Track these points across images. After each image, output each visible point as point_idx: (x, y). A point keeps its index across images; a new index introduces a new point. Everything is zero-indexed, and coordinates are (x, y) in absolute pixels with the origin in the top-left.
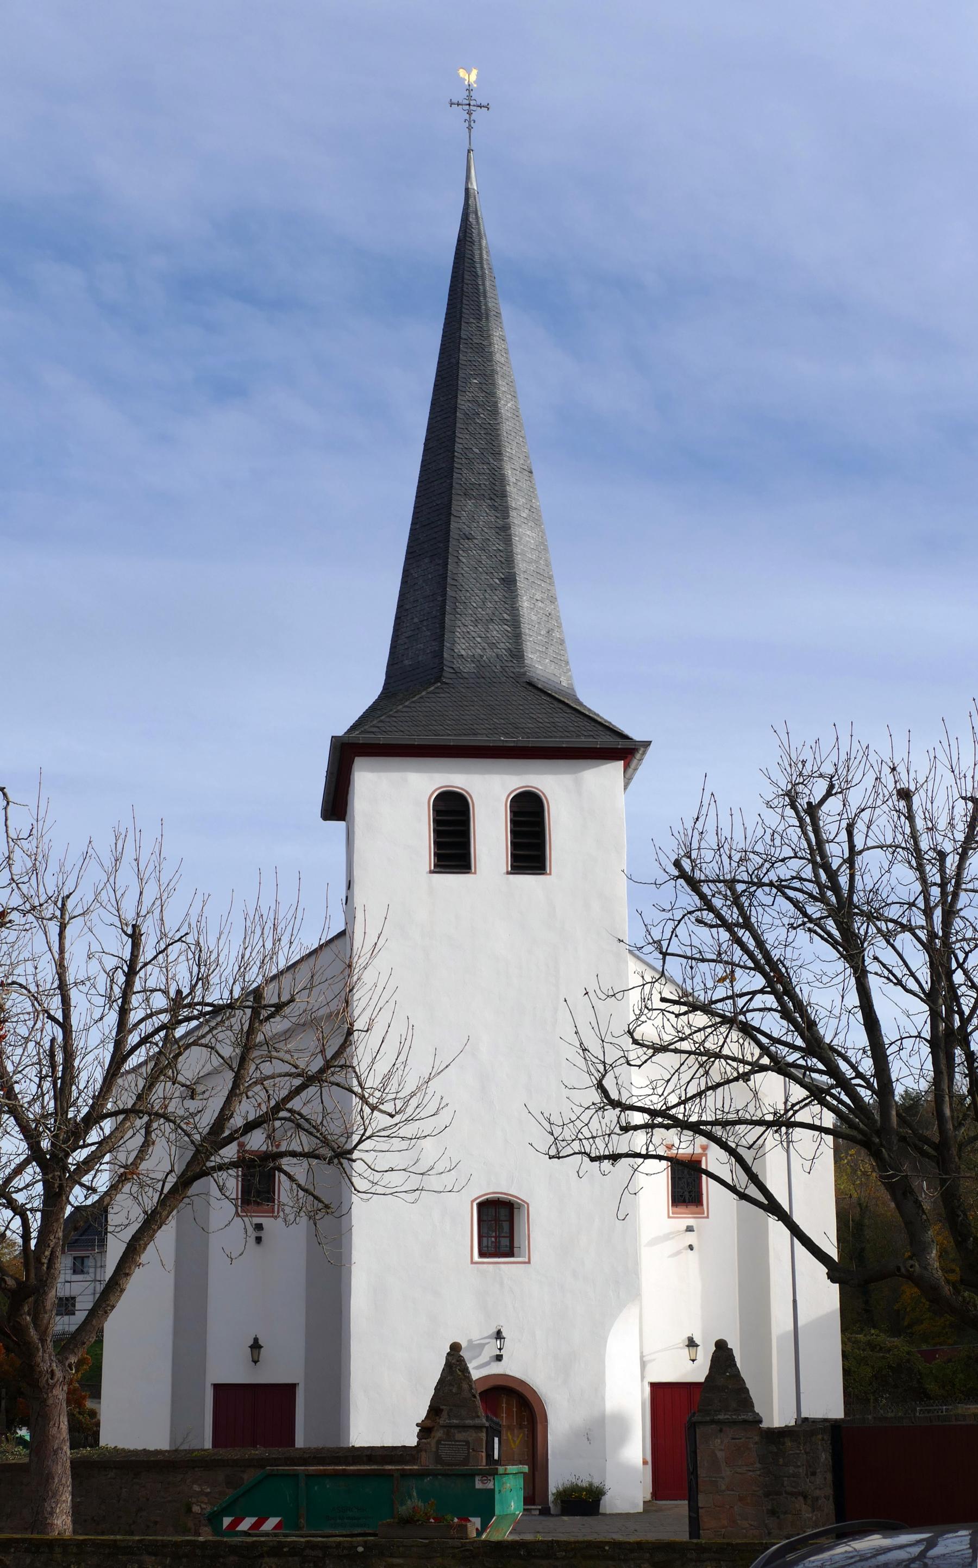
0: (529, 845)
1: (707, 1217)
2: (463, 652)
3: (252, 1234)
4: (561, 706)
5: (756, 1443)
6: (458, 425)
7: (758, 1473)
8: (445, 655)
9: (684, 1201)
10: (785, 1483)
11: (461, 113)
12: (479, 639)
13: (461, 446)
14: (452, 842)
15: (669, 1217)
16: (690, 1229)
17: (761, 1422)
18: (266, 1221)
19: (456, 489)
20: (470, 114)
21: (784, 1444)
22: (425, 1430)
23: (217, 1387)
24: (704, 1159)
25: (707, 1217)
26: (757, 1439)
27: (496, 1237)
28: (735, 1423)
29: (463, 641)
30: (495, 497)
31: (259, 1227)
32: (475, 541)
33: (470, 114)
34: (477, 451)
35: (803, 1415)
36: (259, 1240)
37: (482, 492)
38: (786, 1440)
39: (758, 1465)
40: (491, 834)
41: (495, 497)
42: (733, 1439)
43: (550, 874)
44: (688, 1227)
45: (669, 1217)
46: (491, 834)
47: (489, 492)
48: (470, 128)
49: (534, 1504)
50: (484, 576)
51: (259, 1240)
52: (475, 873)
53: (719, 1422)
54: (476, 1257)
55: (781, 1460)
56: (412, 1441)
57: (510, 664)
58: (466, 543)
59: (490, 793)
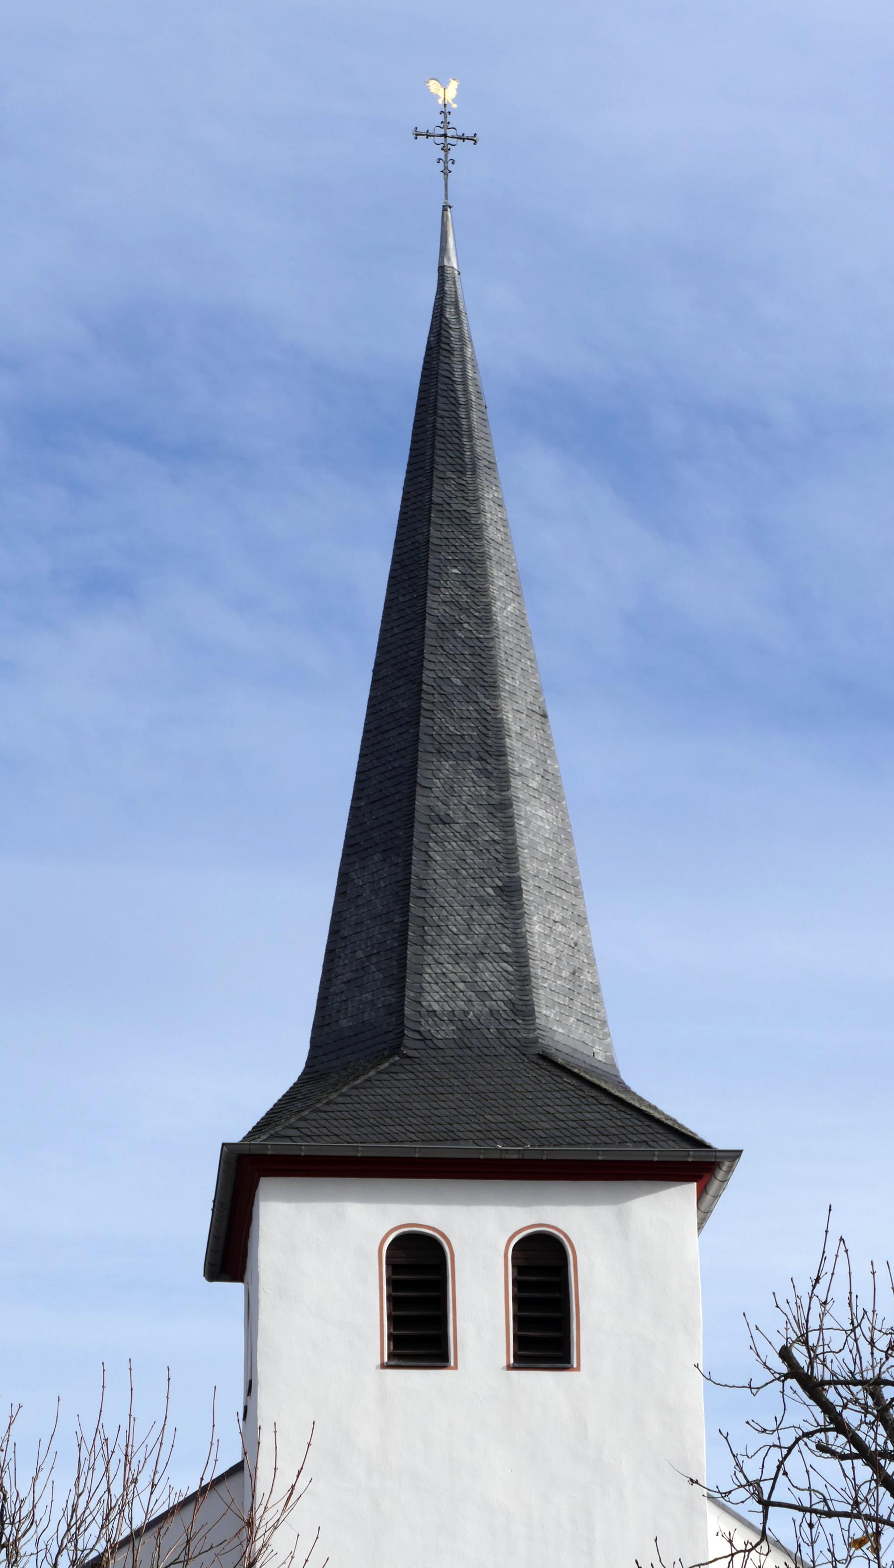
0: (544, 1331)
2: (436, 1007)
4: (594, 1093)
6: (428, 641)
8: (407, 1011)
12: (461, 986)
13: (432, 675)
14: (418, 1326)
30: (487, 757)
32: (456, 827)
40: (481, 1303)
41: (487, 757)
46: (481, 1303)
47: (478, 748)
58: (441, 831)
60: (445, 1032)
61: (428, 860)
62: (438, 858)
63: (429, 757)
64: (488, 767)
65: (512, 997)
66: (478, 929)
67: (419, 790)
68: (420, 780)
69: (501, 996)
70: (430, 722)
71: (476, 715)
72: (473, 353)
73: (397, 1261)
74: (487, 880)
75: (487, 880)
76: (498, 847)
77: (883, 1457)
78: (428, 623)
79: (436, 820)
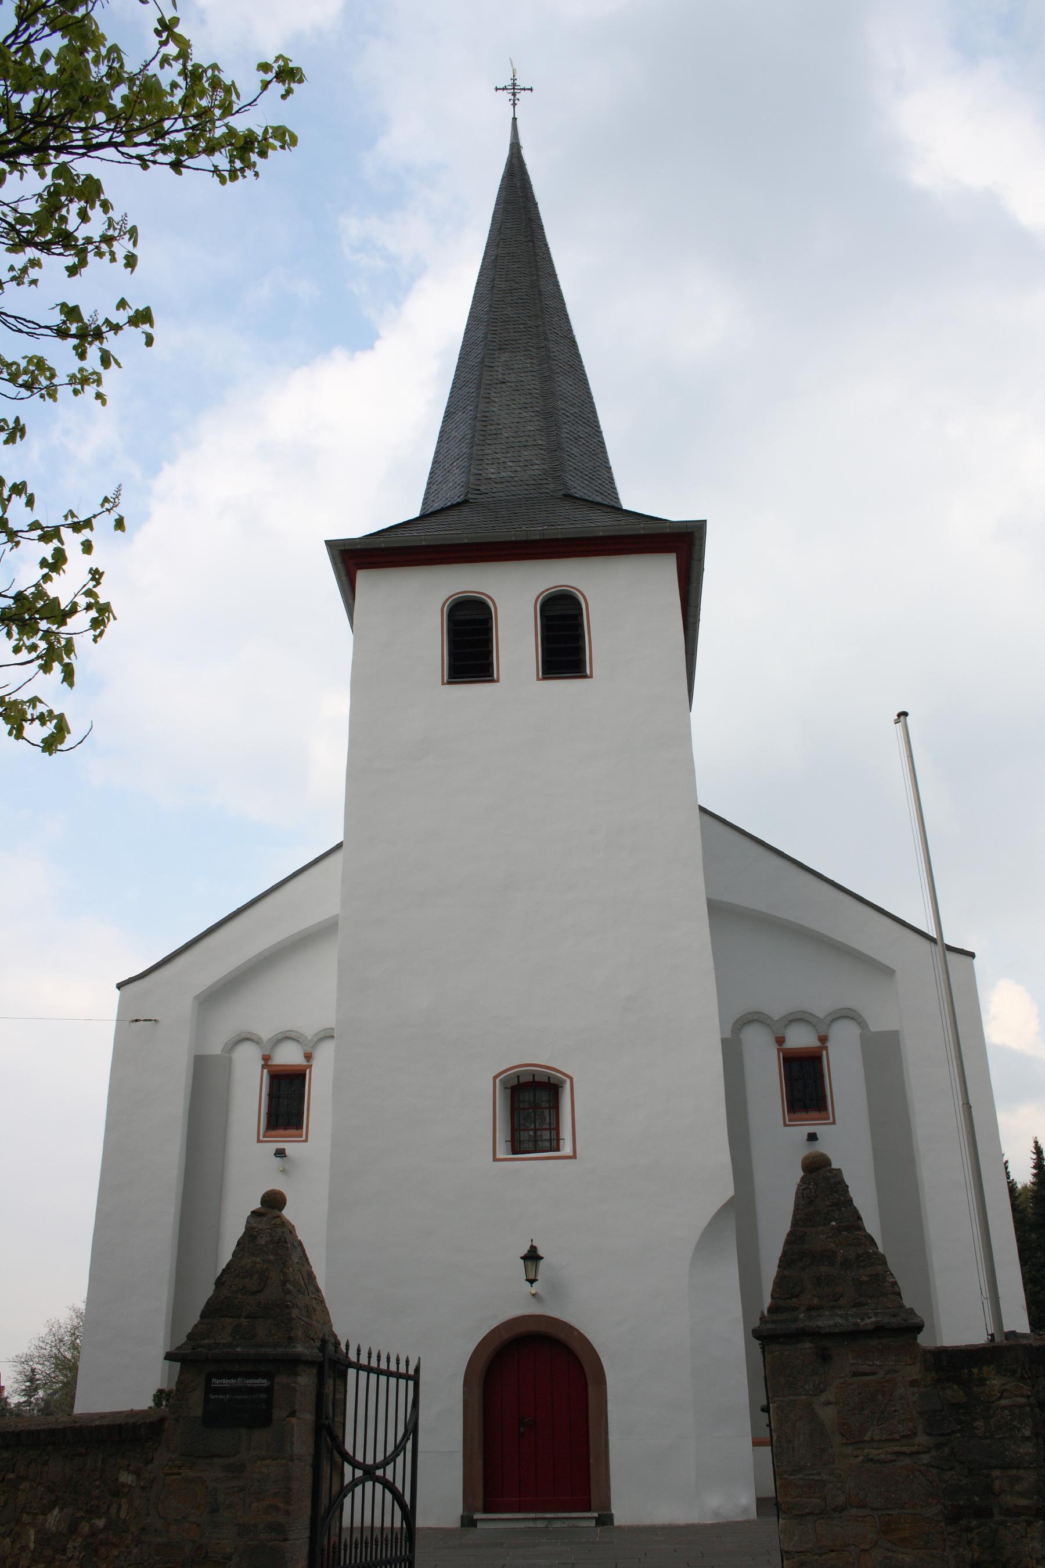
0: (564, 646)
1: (834, 1123)
5: (913, 1383)
7: (925, 1458)
10: (997, 1484)
11: (507, 95)
15: (785, 1125)
17: (919, 1328)
18: (290, 1148)
20: (514, 94)
21: (982, 1382)
24: (824, 1052)
25: (834, 1123)
26: (914, 1372)
27: (535, 1130)
28: (854, 1334)
31: (280, 1153)
33: (514, 94)
35: (1006, 1329)
39: (922, 1439)
40: (517, 640)
42: (855, 1374)
43: (591, 677)
45: (785, 1125)
46: (517, 640)
48: (514, 104)
49: (589, 1510)
53: (815, 1335)
55: (979, 1423)
56: (152, 1404)
59: (515, 598)
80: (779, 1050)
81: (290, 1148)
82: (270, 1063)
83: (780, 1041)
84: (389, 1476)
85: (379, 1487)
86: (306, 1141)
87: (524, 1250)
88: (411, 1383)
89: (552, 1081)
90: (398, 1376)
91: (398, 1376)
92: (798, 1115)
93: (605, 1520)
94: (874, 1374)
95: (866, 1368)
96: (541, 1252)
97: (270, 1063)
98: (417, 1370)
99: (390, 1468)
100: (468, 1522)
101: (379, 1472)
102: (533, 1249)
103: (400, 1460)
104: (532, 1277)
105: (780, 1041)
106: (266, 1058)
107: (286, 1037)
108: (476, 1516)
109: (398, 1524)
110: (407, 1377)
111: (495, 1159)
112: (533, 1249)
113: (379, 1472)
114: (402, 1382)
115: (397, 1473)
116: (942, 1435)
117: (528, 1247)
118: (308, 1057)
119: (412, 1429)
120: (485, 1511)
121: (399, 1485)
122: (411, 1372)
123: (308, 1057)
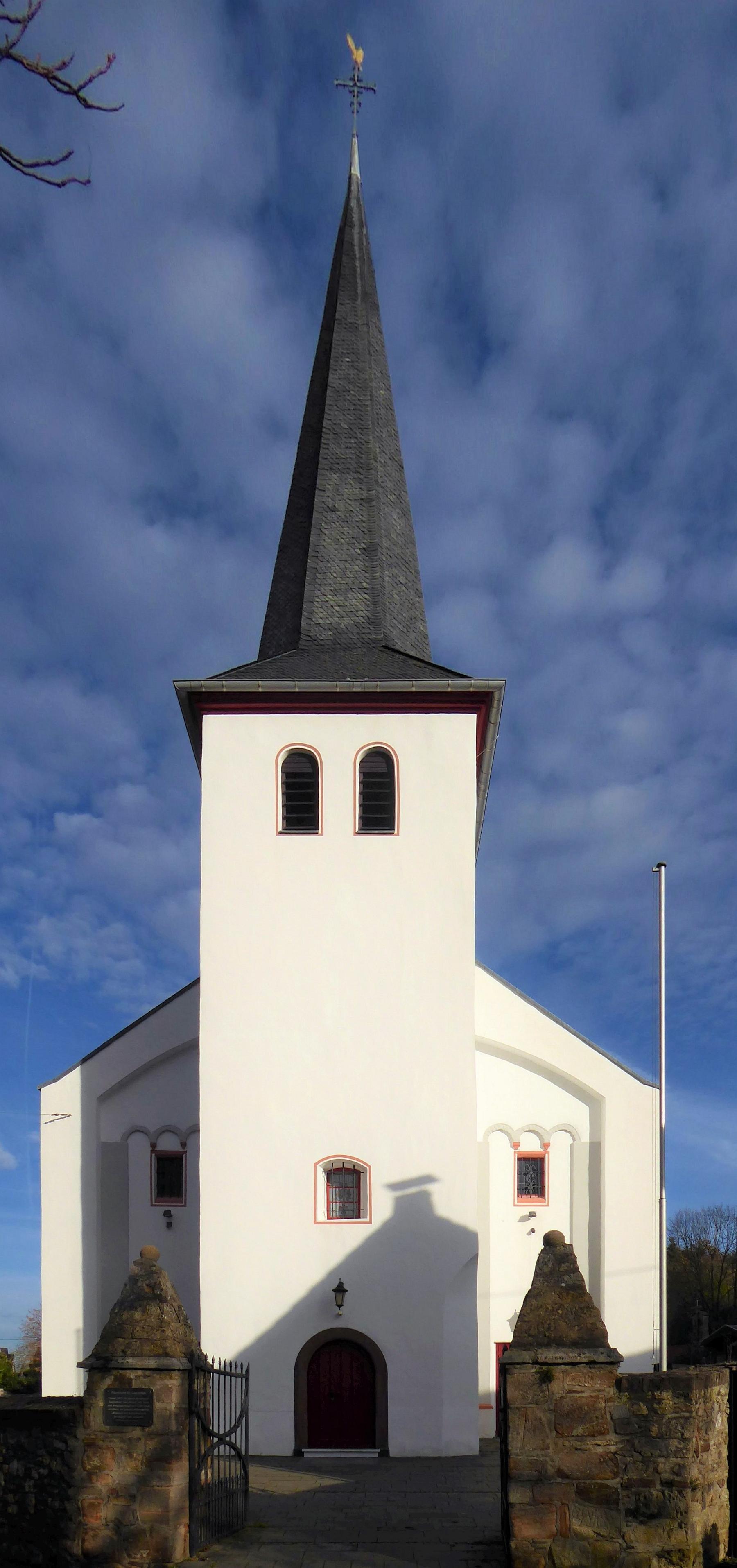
0: (378, 808)
2: (321, 621)
3: (163, 1221)
4: (415, 662)
6: (327, 402)
8: (303, 624)
9: (528, 1193)
12: (337, 608)
13: (329, 422)
14: (300, 805)
15: (515, 1205)
16: (532, 1215)
18: (173, 1210)
19: (322, 463)
21: (660, 1401)
22: (85, 1392)
23: (498, 1345)
29: (322, 610)
30: (361, 470)
31: (167, 1214)
32: (339, 513)
34: (346, 426)
36: (169, 1225)
37: (348, 466)
38: (665, 1395)
40: (339, 794)
41: (361, 470)
44: (530, 1213)
45: (515, 1205)
46: (339, 794)
47: (355, 466)
50: (345, 547)
51: (169, 1225)
52: (322, 834)
54: (322, 1216)
55: (655, 1429)
57: (367, 631)
58: (330, 516)
59: (339, 741)
60: (326, 636)
61: (321, 533)
62: (327, 532)
63: (323, 472)
64: (361, 477)
65: (368, 614)
66: (348, 574)
67: (317, 491)
68: (329, 384)
69: (363, 613)
70: (326, 451)
71: (354, 445)
72: (367, 232)
73: (289, 771)
74: (357, 544)
75: (357, 544)
76: (364, 525)
77: (133, 1308)
78: (328, 392)
79: (327, 510)
80: (515, 1152)
81: (173, 1210)
82: (157, 1149)
83: (516, 1145)
84: (233, 1441)
85: (227, 1447)
86: (185, 1205)
87: (335, 1286)
88: (244, 1380)
89: (356, 1168)
90: (237, 1376)
91: (237, 1376)
92: (525, 1198)
93: (385, 1453)
94: (582, 1392)
95: (578, 1388)
96: (345, 1287)
97: (157, 1149)
98: (247, 1371)
99: (233, 1436)
100: (298, 1453)
101: (228, 1439)
102: (341, 1285)
103: (239, 1430)
104: (340, 1303)
105: (516, 1145)
106: (153, 1146)
107: (168, 1130)
108: (303, 1450)
109: (238, 1472)
110: (242, 1376)
111: (315, 1223)
112: (341, 1285)
113: (228, 1439)
114: (239, 1379)
115: (237, 1438)
116: (627, 1435)
117: (337, 1284)
118: (184, 1145)
119: (244, 1413)
120: (310, 1447)
121: (238, 1445)
122: (244, 1373)
123: (184, 1145)
